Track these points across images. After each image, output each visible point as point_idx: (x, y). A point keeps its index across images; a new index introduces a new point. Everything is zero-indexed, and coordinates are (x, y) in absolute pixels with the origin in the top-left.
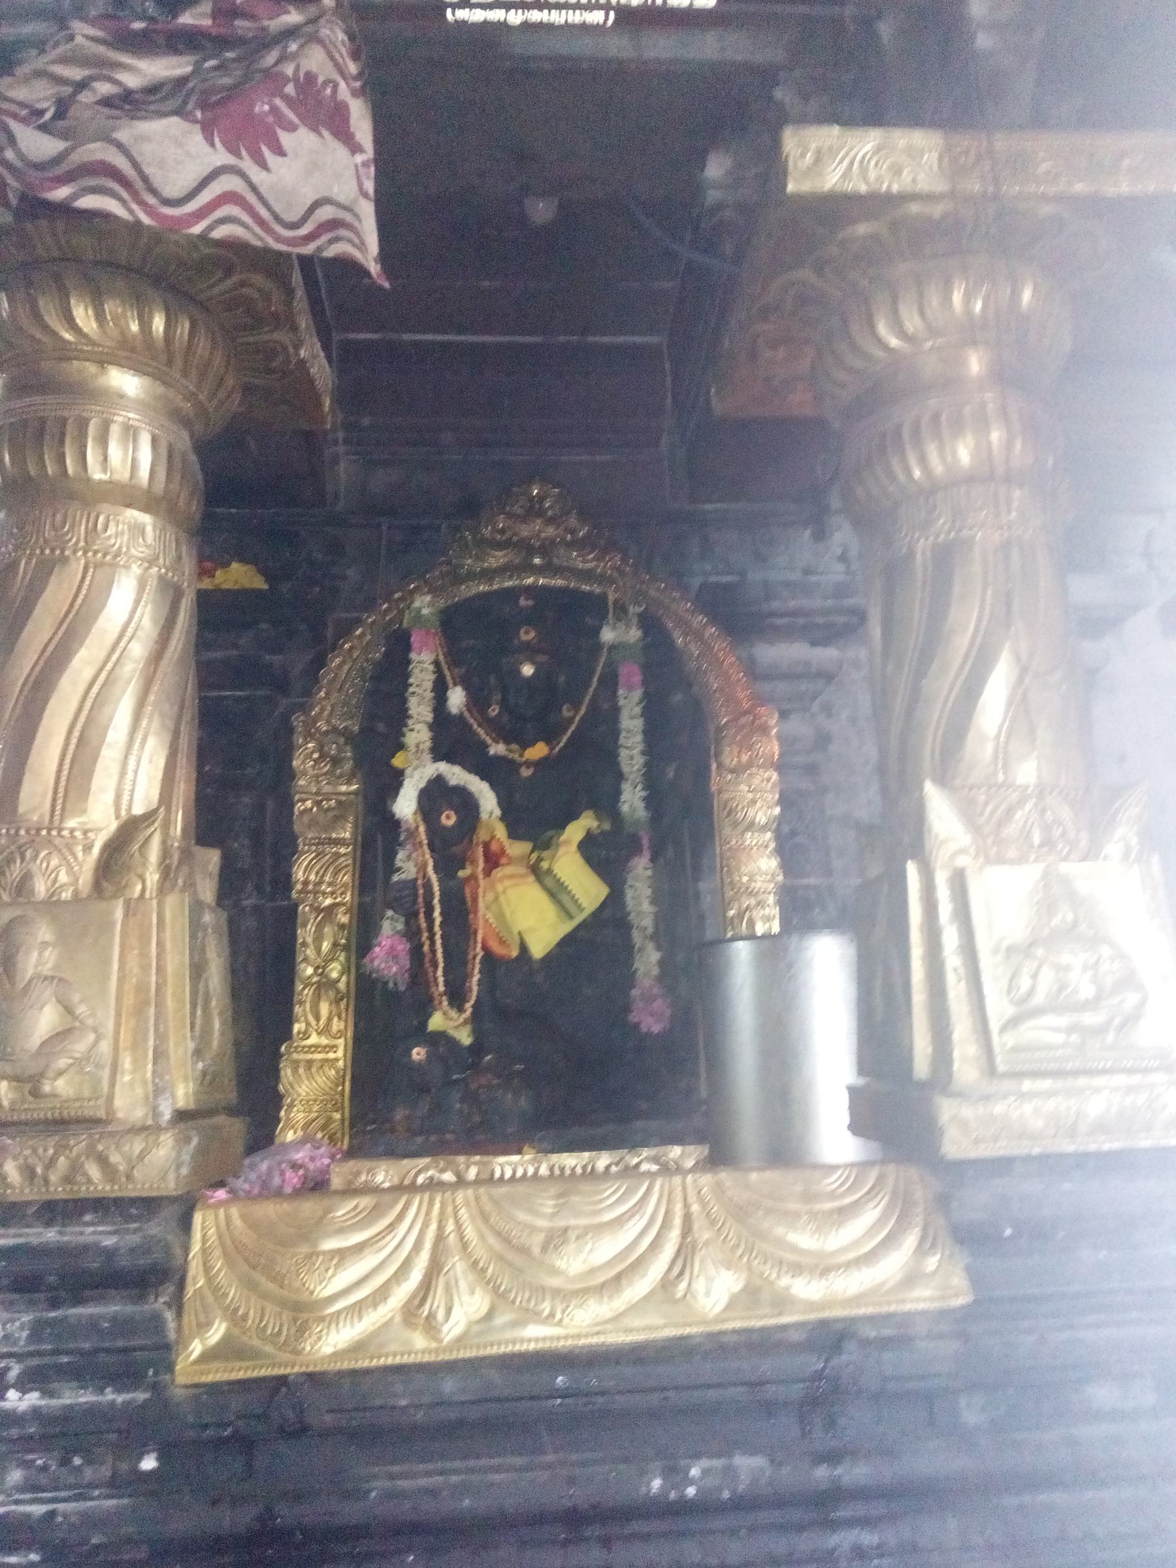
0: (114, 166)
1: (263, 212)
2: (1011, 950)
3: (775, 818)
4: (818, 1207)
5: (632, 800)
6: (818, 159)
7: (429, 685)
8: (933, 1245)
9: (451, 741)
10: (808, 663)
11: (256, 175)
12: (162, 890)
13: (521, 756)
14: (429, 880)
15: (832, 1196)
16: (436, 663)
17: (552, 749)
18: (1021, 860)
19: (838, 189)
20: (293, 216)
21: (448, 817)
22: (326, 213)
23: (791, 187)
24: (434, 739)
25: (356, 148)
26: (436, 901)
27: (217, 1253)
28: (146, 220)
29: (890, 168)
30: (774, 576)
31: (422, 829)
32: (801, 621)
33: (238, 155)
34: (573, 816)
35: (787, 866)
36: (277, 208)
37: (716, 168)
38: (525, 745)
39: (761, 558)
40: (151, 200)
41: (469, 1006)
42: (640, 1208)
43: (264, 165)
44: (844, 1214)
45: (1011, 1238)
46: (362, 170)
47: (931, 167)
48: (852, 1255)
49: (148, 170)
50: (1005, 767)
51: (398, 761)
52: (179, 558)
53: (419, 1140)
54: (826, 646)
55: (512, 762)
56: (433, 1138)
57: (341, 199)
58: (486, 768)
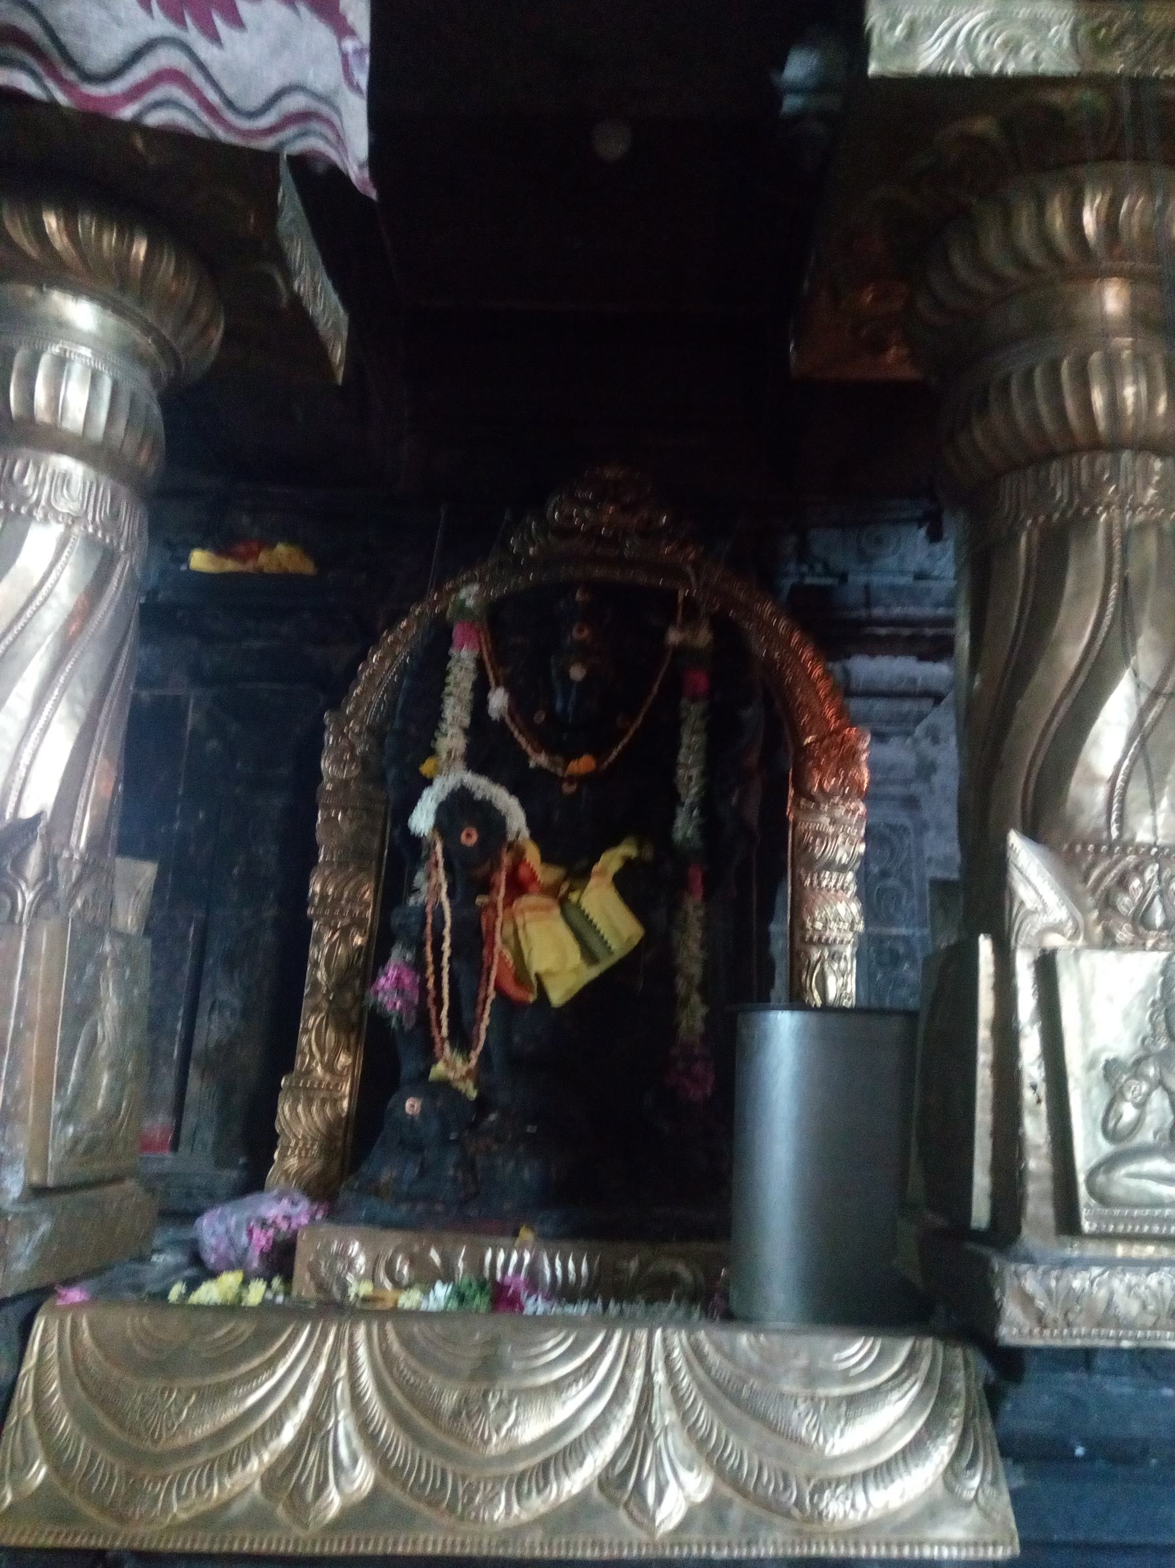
0: (15, 27)
1: (212, 96)
2: (1111, 1070)
3: (859, 856)
4: (821, 1392)
5: (685, 827)
6: (911, 33)
7: (467, 685)
8: (971, 1465)
9: (488, 749)
10: (913, 681)
11: (205, 50)
12: (36, 912)
13: (565, 769)
14: (441, 906)
15: (846, 1377)
16: (479, 662)
17: (598, 764)
18: (1138, 944)
19: (935, 69)
20: (254, 101)
21: (469, 835)
22: (295, 103)
23: (873, 68)
24: (469, 747)
25: (342, 29)
26: (446, 932)
27: (55, 1371)
28: (61, 98)
29: (1005, 44)
30: (876, 580)
31: (439, 848)
32: (906, 632)
33: (180, 21)
34: (615, 843)
35: (870, 912)
36: (230, 91)
37: (799, 67)
38: (571, 756)
39: (865, 558)
40: (71, 76)
41: (474, 1056)
42: (588, 1371)
43: (215, 38)
44: (855, 1404)
45: (1083, 1459)
46: (352, 60)
47: (1060, 42)
48: (859, 1467)
49: (64, 37)
50: (1121, 819)
51: (426, 768)
52: (115, 515)
53: (404, 1208)
54: (935, 661)
55: (555, 775)
56: (420, 1208)
57: (319, 87)
58: (522, 784)
